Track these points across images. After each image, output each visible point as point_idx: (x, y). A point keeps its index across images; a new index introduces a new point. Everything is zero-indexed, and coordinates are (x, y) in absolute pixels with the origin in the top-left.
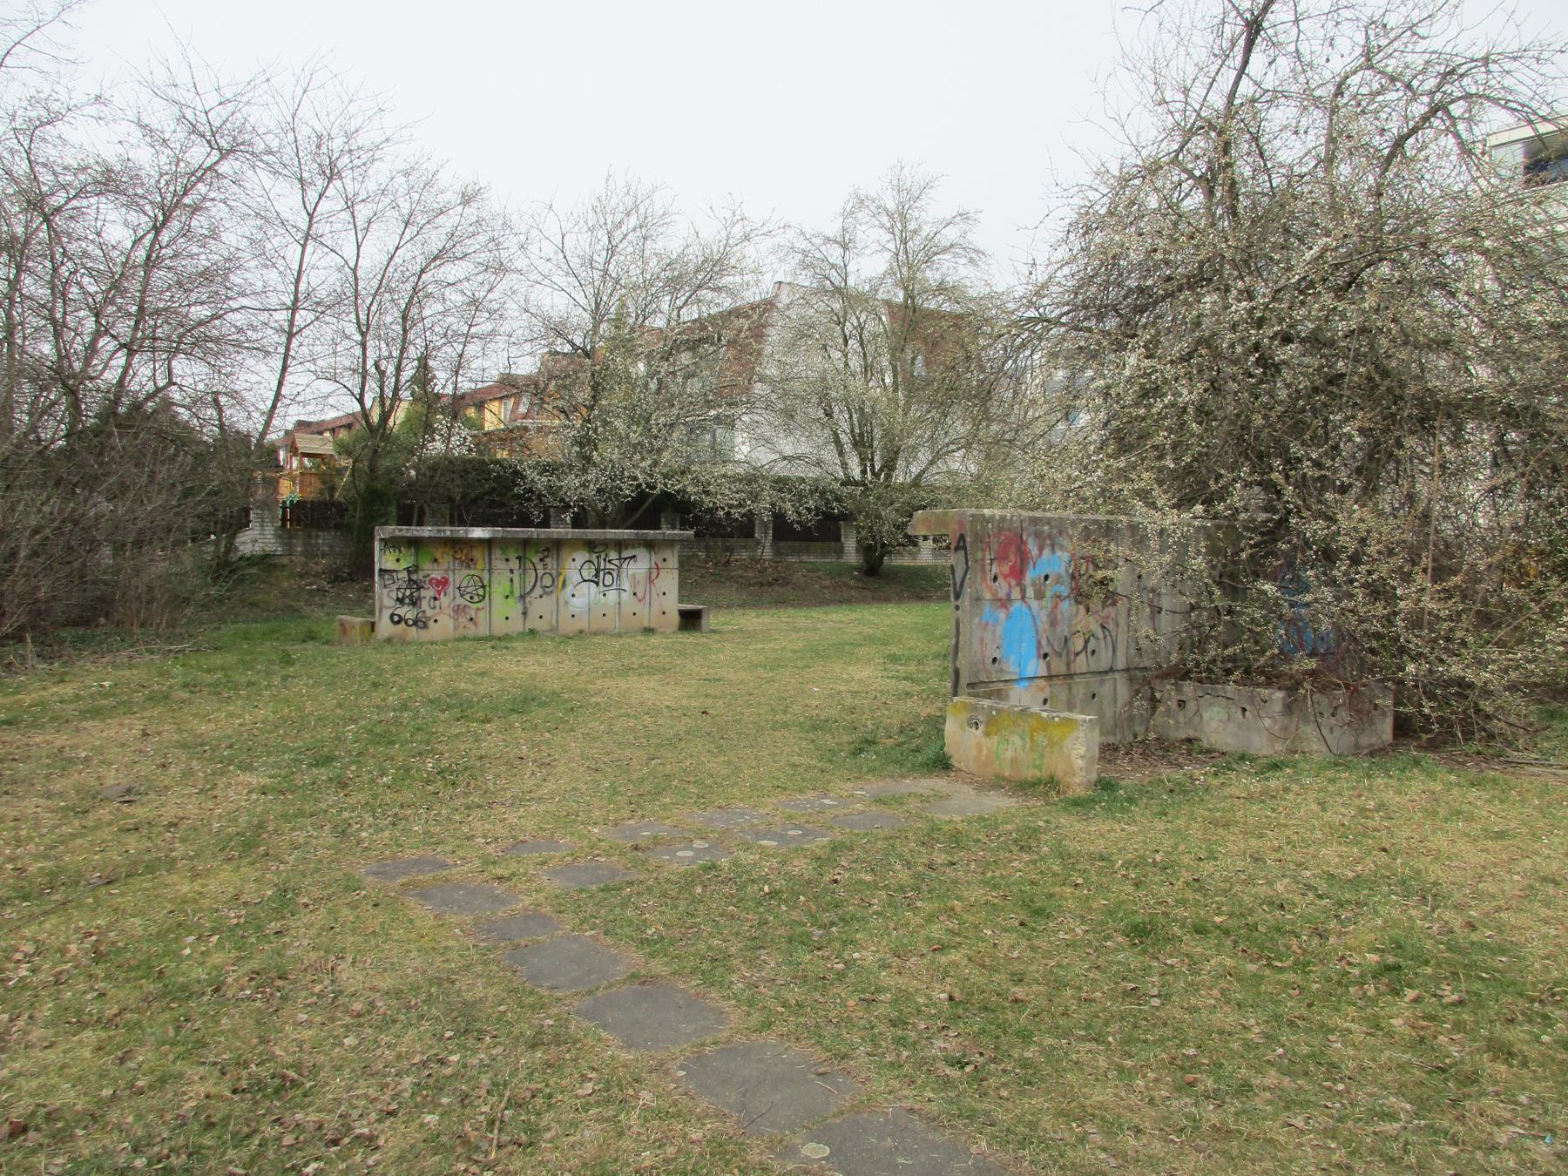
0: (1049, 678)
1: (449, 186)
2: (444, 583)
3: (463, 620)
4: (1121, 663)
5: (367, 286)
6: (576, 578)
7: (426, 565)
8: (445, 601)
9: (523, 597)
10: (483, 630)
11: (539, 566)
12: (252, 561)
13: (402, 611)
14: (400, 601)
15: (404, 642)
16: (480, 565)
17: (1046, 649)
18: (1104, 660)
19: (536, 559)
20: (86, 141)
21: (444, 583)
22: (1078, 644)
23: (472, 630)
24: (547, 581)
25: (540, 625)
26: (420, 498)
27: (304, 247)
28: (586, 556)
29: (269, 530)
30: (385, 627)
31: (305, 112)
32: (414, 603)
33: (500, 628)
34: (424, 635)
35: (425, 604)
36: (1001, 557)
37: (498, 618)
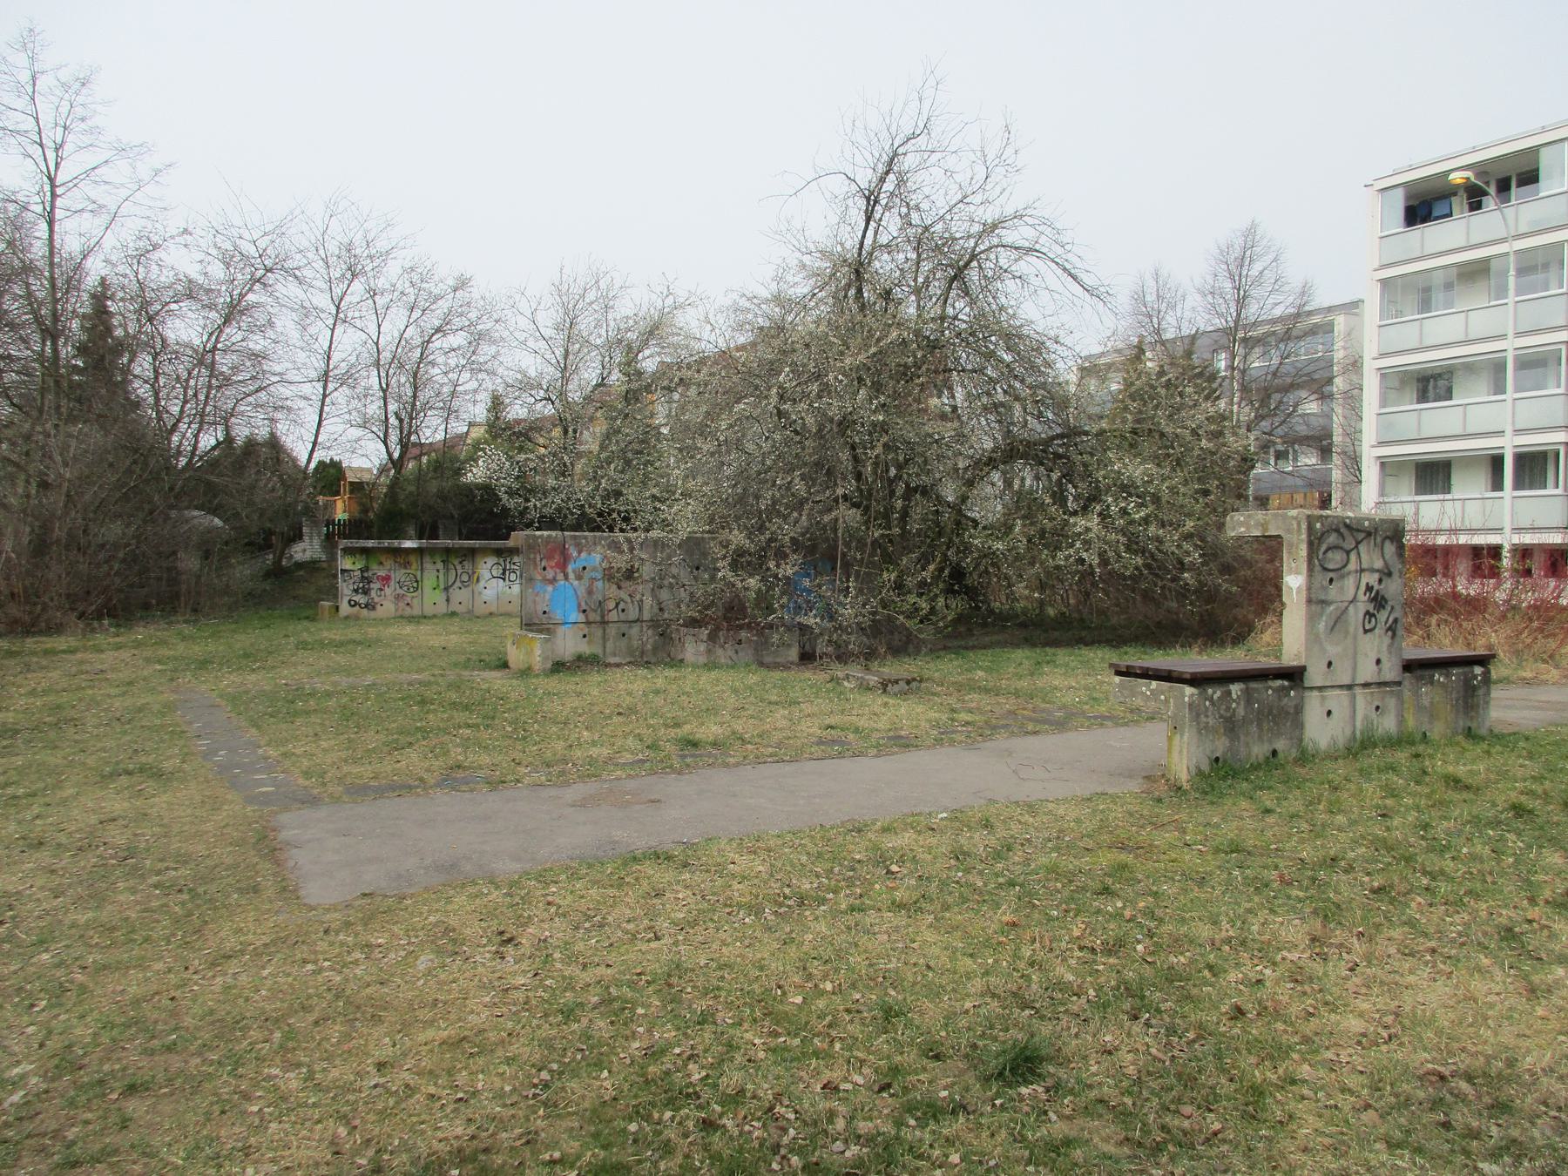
0: (588, 623)
1: (445, 275)
2: (387, 579)
3: (402, 604)
4: (646, 616)
5: (386, 356)
6: (487, 575)
7: (374, 566)
8: (388, 591)
9: (446, 589)
10: (416, 611)
11: (459, 567)
12: (300, 565)
13: (357, 598)
14: (356, 591)
15: (357, 618)
16: (414, 566)
17: (584, 607)
18: (633, 613)
19: (456, 562)
20: (179, 263)
21: (387, 579)
22: (612, 605)
23: (408, 612)
24: (465, 577)
25: (460, 609)
26: (441, 511)
27: (333, 331)
28: (495, 560)
29: (316, 542)
30: (345, 608)
31: (335, 227)
32: (366, 592)
33: (429, 610)
34: (373, 614)
35: (373, 593)
36: (549, 557)
37: (428, 602)
